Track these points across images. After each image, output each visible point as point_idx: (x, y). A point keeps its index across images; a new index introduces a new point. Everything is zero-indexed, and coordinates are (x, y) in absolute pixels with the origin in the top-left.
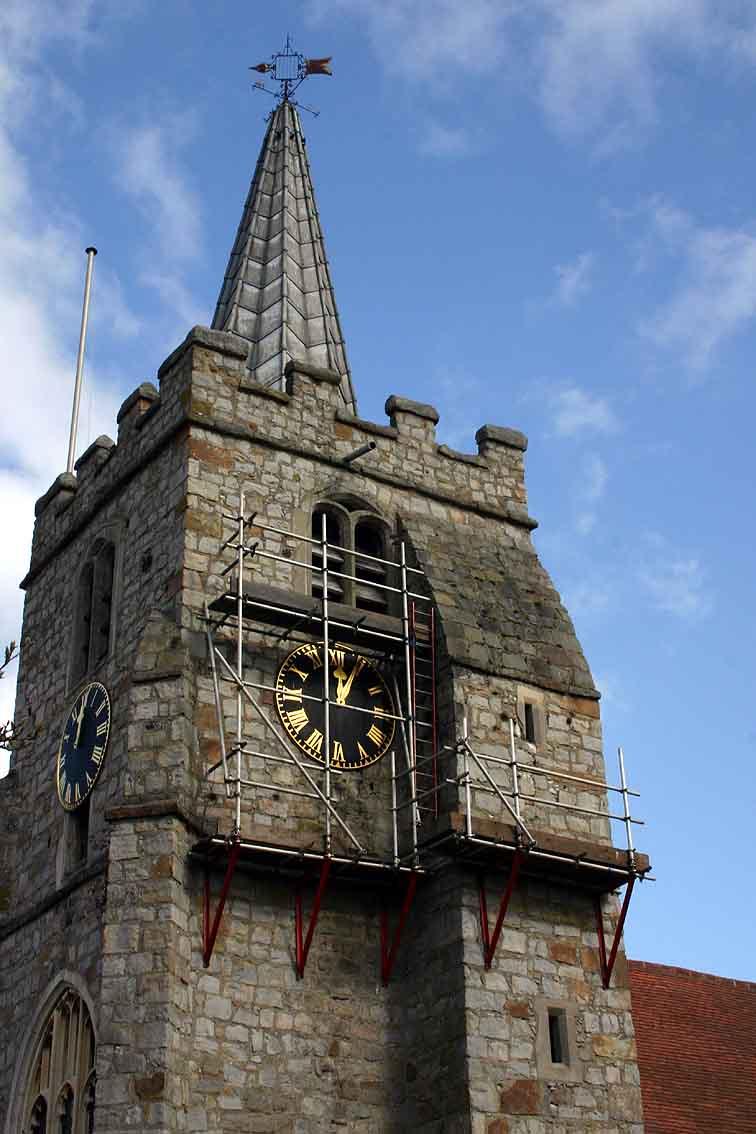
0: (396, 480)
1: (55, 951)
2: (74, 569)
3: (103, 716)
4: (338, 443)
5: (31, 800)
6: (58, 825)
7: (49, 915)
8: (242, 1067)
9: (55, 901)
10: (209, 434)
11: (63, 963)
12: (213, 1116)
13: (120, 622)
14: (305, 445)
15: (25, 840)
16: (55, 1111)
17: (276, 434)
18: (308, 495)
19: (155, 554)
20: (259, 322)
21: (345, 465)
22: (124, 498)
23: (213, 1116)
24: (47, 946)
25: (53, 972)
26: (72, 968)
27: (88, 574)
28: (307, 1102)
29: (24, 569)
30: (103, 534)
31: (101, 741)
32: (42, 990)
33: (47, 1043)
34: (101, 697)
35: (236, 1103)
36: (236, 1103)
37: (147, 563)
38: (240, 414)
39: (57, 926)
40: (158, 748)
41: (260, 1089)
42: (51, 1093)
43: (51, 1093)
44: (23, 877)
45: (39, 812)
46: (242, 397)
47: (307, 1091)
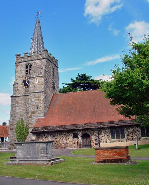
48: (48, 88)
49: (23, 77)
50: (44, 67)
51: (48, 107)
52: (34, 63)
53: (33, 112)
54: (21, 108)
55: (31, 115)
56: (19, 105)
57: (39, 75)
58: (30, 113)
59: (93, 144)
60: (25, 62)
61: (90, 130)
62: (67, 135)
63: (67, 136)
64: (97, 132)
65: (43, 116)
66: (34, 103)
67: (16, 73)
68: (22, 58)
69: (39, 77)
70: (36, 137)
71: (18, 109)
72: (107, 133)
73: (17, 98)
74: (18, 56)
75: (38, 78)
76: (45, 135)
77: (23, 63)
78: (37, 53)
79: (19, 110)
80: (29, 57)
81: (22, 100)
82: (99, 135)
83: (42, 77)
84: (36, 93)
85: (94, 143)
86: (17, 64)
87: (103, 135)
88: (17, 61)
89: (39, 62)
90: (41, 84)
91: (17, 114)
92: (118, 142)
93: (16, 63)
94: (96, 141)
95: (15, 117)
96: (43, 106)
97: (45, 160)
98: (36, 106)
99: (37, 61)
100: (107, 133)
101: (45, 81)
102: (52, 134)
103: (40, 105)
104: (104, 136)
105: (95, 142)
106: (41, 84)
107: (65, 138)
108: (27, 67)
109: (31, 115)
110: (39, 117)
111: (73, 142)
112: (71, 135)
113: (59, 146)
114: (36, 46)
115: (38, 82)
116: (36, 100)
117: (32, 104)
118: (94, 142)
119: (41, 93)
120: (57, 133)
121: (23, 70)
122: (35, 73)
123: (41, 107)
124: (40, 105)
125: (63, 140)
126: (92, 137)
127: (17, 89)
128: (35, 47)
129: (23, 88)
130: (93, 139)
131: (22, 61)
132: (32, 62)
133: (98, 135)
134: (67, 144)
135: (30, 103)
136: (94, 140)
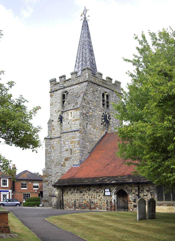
48: (90, 124)
49: (59, 111)
50: (82, 95)
51: (90, 151)
52: (72, 89)
53: (66, 159)
54: (57, 154)
55: (64, 163)
56: (55, 150)
57: (73, 107)
58: (63, 160)
59: (131, 206)
60: (61, 90)
61: (126, 186)
62: (98, 191)
63: (97, 192)
64: (137, 188)
65: (79, 164)
66: (68, 147)
67: (52, 106)
68: (57, 85)
69: (74, 109)
70: (60, 192)
71: (54, 155)
72: (151, 191)
73: (52, 140)
74: (53, 81)
75: (73, 110)
76: (70, 191)
77: (59, 91)
78: (75, 74)
79: (55, 157)
80: (66, 82)
81: (58, 143)
82: (139, 193)
83: (78, 109)
84: (70, 133)
85: (132, 205)
86: (52, 93)
87: (145, 194)
88: (51, 90)
89: (77, 88)
90: (76, 120)
91: (53, 161)
92: (168, 206)
93: (50, 92)
94: (135, 202)
95: (50, 166)
96: (78, 151)
97: (130, 225)
98: (69, 151)
99: (76, 86)
100: (151, 191)
101: (82, 114)
102: (79, 190)
103: (74, 149)
104: (147, 195)
105: (133, 203)
106: (76, 120)
107: (95, 196)
108: (64, 96)
109: (64, 163)
110: (74, 165)
111: (104, 201)
112: (102, 192)
113: (87, 206)
114: (80, 63)
115: (72, 118)
116: (70, 142)
117: (65, 148)
118: (132, 204)
119: (76, 132)
120: (85, 188)
121: (59, 101)
122: (69, 104)
123: (75, 151)
124: (74, 149)
125: (92, 198)
126: (130, 196)
127: (53, 129)
128: (79, 66)
129: (60, 127)
130: (130, 199)
131: (58, 88)
132: (69, 88)
133: (137, 193)
134: (97, 203)
135: (63, 147)
136: (132, 201)
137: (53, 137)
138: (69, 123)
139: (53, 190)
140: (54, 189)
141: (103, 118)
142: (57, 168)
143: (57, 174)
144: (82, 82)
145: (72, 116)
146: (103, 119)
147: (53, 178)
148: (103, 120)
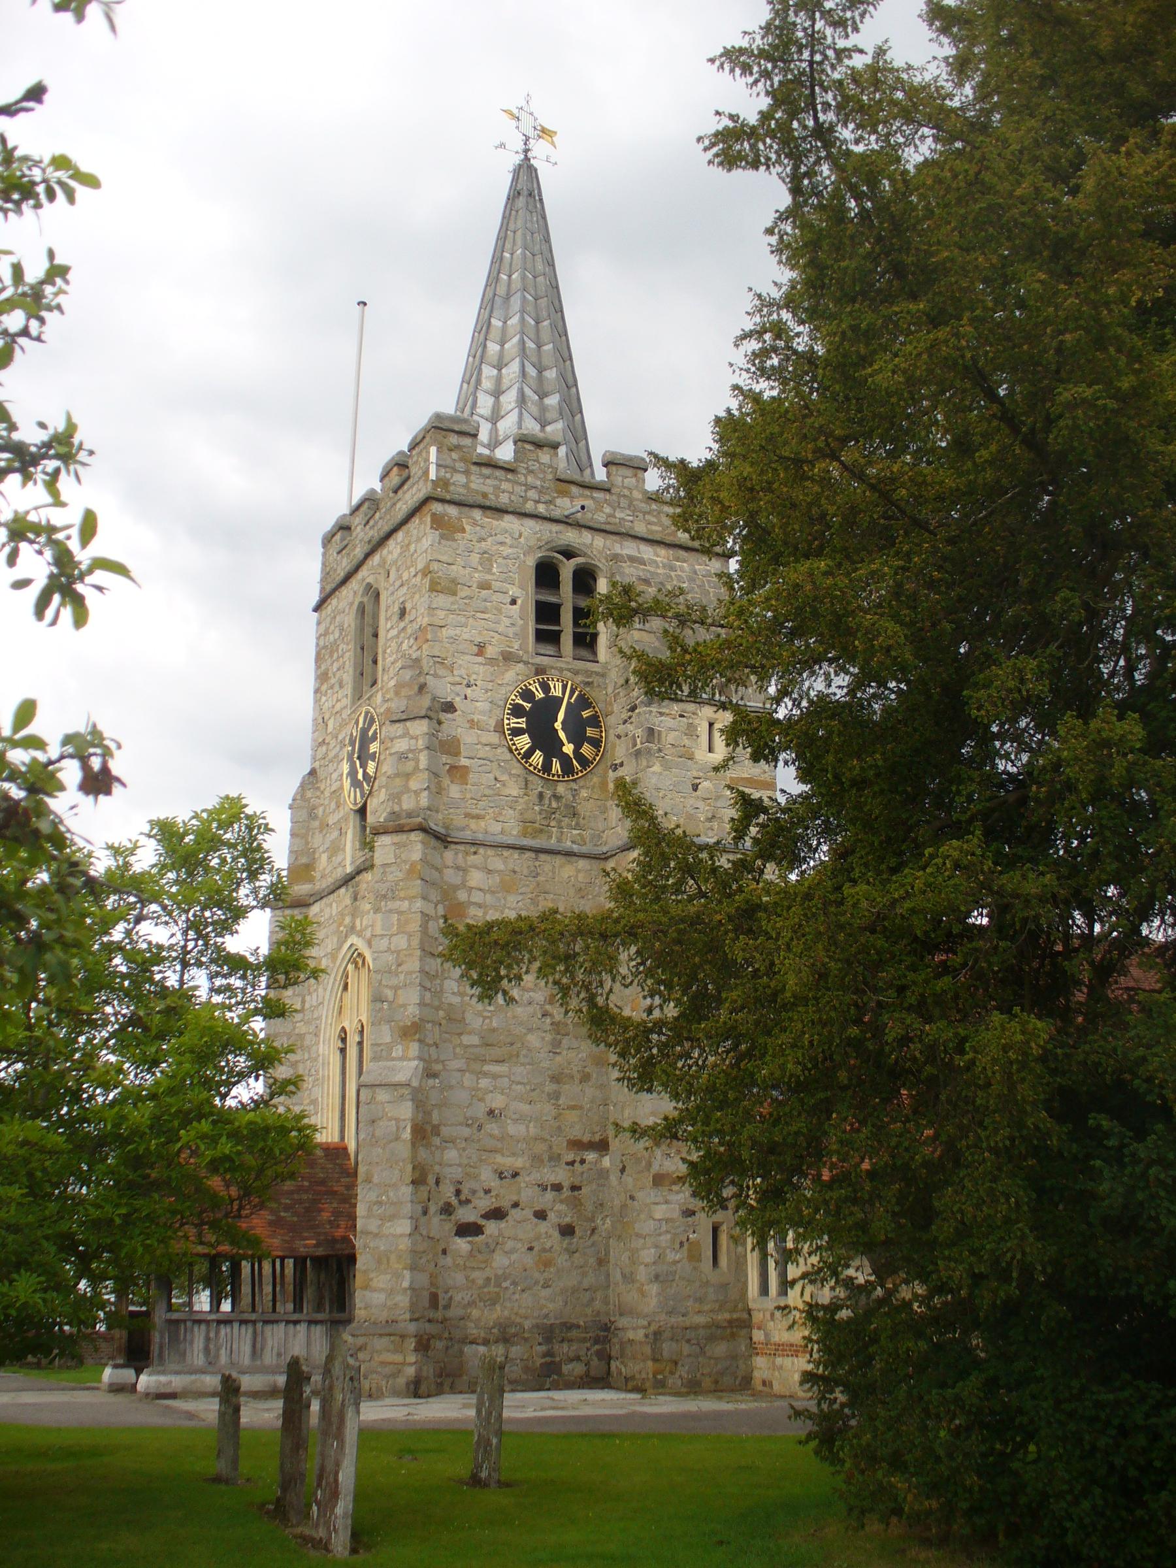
0: (608, 527)
1: (348, 920)
2: (352, 604)
3: (374, 738)
4: (559, 501)
5: (327, 794)
6: (345, 819)
7: (343, 890)
8: (479, 1014)
9: (348, 880)
10: (446, 506)
11: (352, 929)
12: (458, 1050)
13: (384, 659)
14: (529, 507)
15: (324, 826)
16: (352, 1039)
17: (504, 499)
18: (529, 550)
19: (408, 606)
20: (499, 379)
21: (566, 521)
22: (385, 552)
23: (458, 1050)
24: (342, 914)
25: (346, 937)
26: (359, 935)
27: (362, 610)
28: (530, 1037)
29: (315, 598)
30: (370, 580)
31: (373, 757)
32: (340, 948)
33: (346, 987)
34: (372, 721)
35: (475, 1040)
36: (475, 1040)
37: (403, 613)
38: (473, 486)
39: (348, 901)
40: (408, 776)
41: (494, 1030)
42: (350, 1025)
43: (350, 1025)
44: (324, 857)
45: (333, 806)
46: (474, 468)
47: (530, 1030)
80: (574, 489)
121: (513, 591)
137: (467, 835)
138: (695, 788)
139: (444, 1252)
140: (458, 1240)
141: (522, 723)
142: (495, 1077)
143: (492, 1128)
144: (603, 527)
145: (388, 679)
146: (517, 732)
147: (451, 1155)
148: (524, 741)
